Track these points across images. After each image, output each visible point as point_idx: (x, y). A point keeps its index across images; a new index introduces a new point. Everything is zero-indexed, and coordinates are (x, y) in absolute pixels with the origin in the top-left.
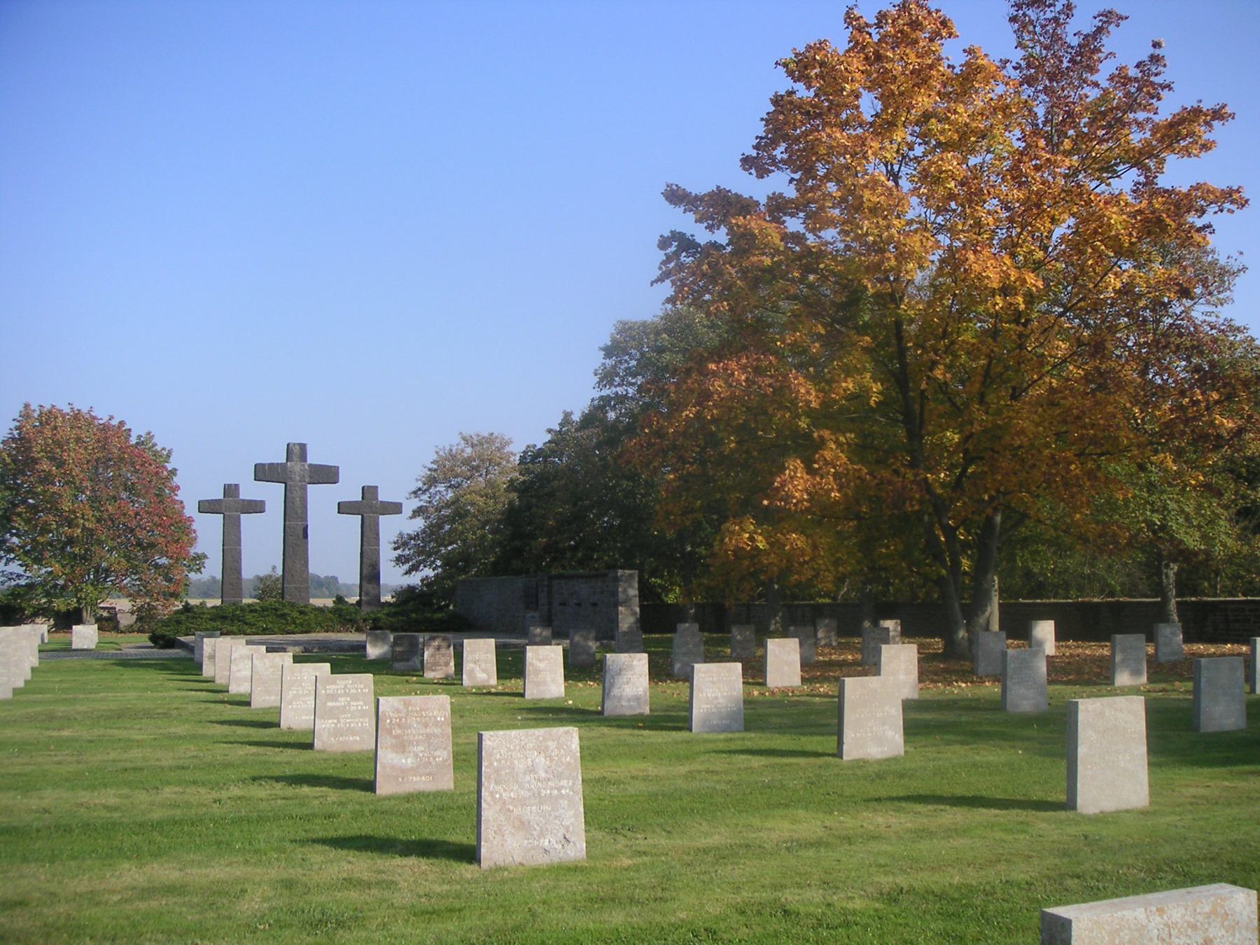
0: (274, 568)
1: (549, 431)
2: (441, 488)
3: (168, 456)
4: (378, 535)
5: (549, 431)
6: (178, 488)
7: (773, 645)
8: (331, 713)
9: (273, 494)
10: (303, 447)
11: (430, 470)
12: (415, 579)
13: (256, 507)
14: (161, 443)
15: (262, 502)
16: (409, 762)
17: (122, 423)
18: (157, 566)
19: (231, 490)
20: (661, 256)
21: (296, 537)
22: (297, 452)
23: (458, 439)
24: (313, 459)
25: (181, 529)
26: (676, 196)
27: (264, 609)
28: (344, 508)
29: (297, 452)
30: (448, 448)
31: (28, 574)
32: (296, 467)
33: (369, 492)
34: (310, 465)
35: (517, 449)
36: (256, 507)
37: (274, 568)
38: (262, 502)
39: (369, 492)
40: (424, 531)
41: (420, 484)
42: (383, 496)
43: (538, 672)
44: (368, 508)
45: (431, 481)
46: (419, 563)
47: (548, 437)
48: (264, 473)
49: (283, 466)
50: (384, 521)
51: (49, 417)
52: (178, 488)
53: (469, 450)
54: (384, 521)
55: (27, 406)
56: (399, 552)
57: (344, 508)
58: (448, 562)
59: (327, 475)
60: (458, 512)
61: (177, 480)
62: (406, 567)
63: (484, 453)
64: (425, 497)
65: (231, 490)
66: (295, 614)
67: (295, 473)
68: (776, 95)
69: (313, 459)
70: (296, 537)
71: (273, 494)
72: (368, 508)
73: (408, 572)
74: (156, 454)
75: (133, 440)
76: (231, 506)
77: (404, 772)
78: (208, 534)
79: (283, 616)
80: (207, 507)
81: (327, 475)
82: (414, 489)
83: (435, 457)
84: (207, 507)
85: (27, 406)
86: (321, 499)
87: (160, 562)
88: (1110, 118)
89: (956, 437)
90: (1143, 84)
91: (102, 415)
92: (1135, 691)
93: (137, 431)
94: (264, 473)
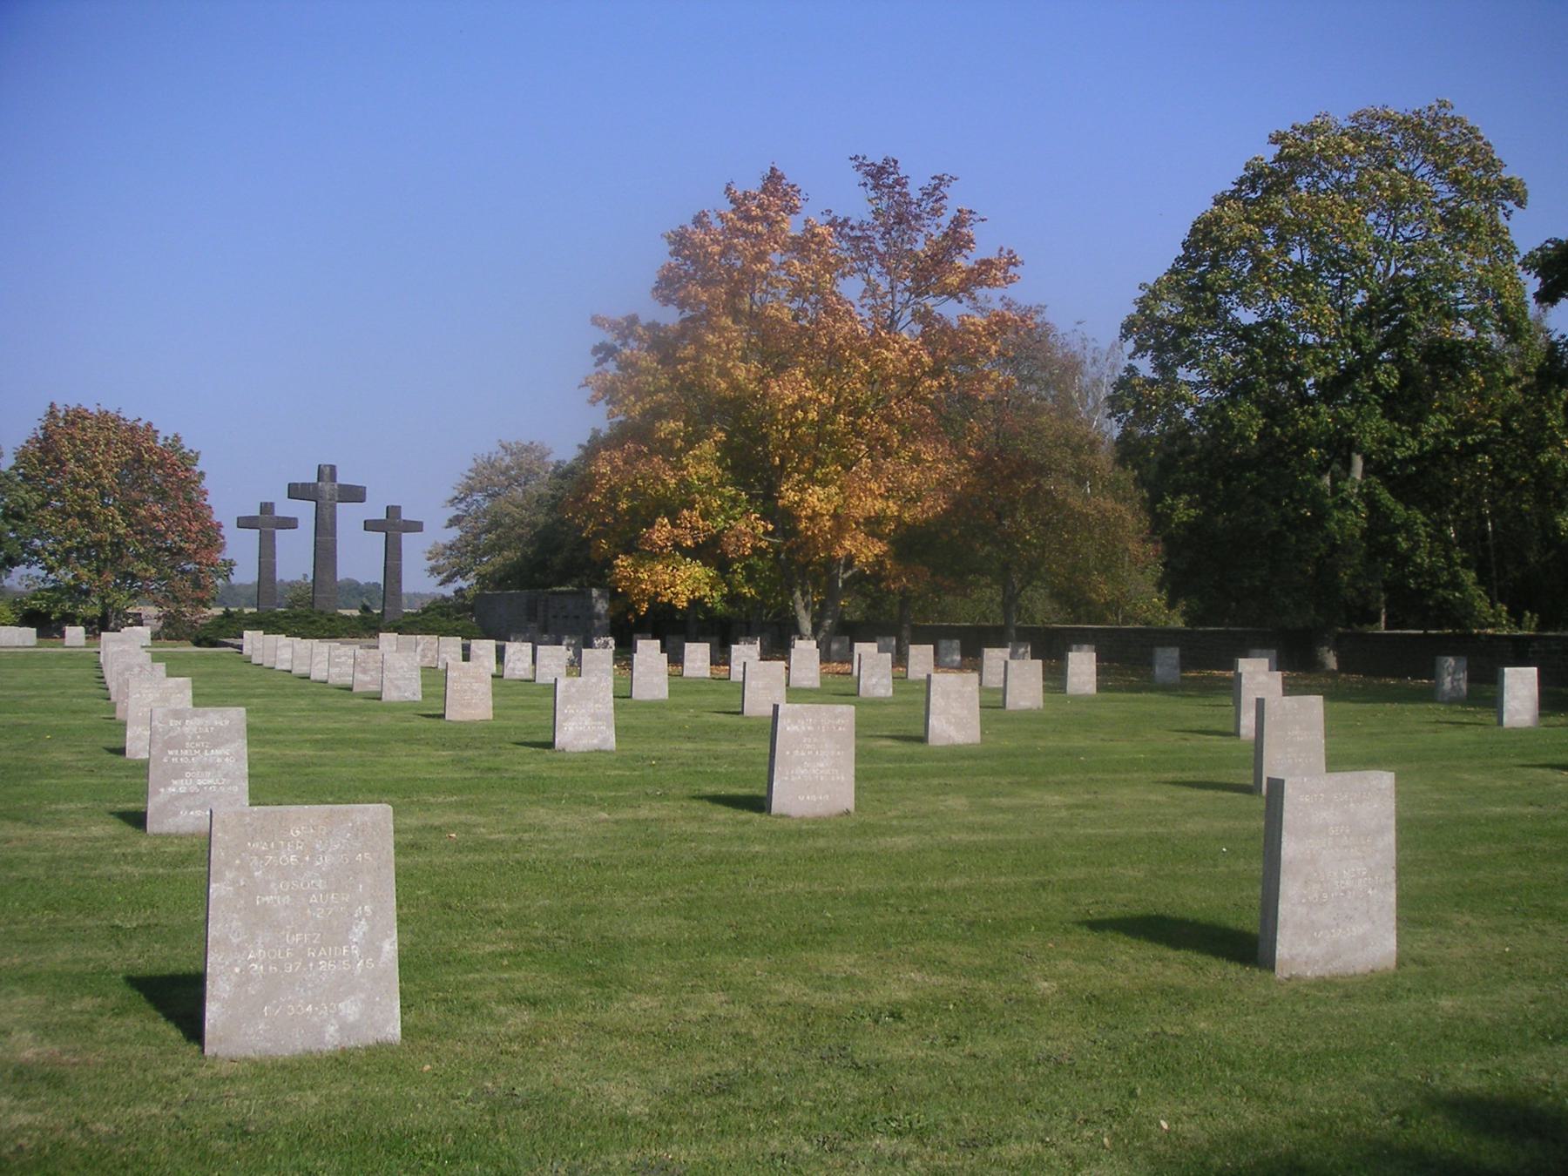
0: (305, 576)
6: (206, 493)
7: (689, 647)
8: (337, 665)
9: (304, 511)
10: (333, 468)
12: (449, 591)
13: (290, 523)
14: (188, 445)
15: (295, 519)
16: (368, 678)
17: (150, 425)
18: (183, 572)
19: (267, 508)
20: (595, 360)
21: (325, 552)
22: (327, 472)
24: (342, 479)
25: (211, 537)
26: (596, 321)
27: (295, 616)
28: (370, 526)
29: (327, 472)
31: (52, 576)
32: (326, 487)
33: (393, 511)
35: (552, 459)
36: (290, 523)
37: (305, 576)
38: (295, 519)
39: (393, 511)
41: (456, 493)
42: (405, 516)
43: (478, 657)
44: (393, 526)
45: (471, 490)
47: (581, 452)
48: (297, 491)
50: (406, 538)
51: (77, 418)
52: (206, 493)
53: (508, 459)
54: (406, 538)
56: (433, 562)
57: (370, 526)
59: (355, 494)
61: (205, 485)
64: (462, 506)
65: (267, 508)
66: (324, 621)
67: (326, 493)
68: (333, 468)
69: (342, 479)
70: (325, 552)
71: (304, 511)
72: (393, 526)
74: (184, 457)
75: (161, 442)
76: (266, 523)
77: (366, 683)
78: (241, 549)
79: (313, 622)
80: (245, 523)
81: (355, 494)
82: (450, 497)
83: (474, 465)
84: (245, 523)
85: (52, 405)
86: (349, 517)
87: (187, 567)
88: (940, 258)
89: (792, 496)
90: (956, 239)
91: (129, 415)
93: (165, 431)
94: (297, 491)
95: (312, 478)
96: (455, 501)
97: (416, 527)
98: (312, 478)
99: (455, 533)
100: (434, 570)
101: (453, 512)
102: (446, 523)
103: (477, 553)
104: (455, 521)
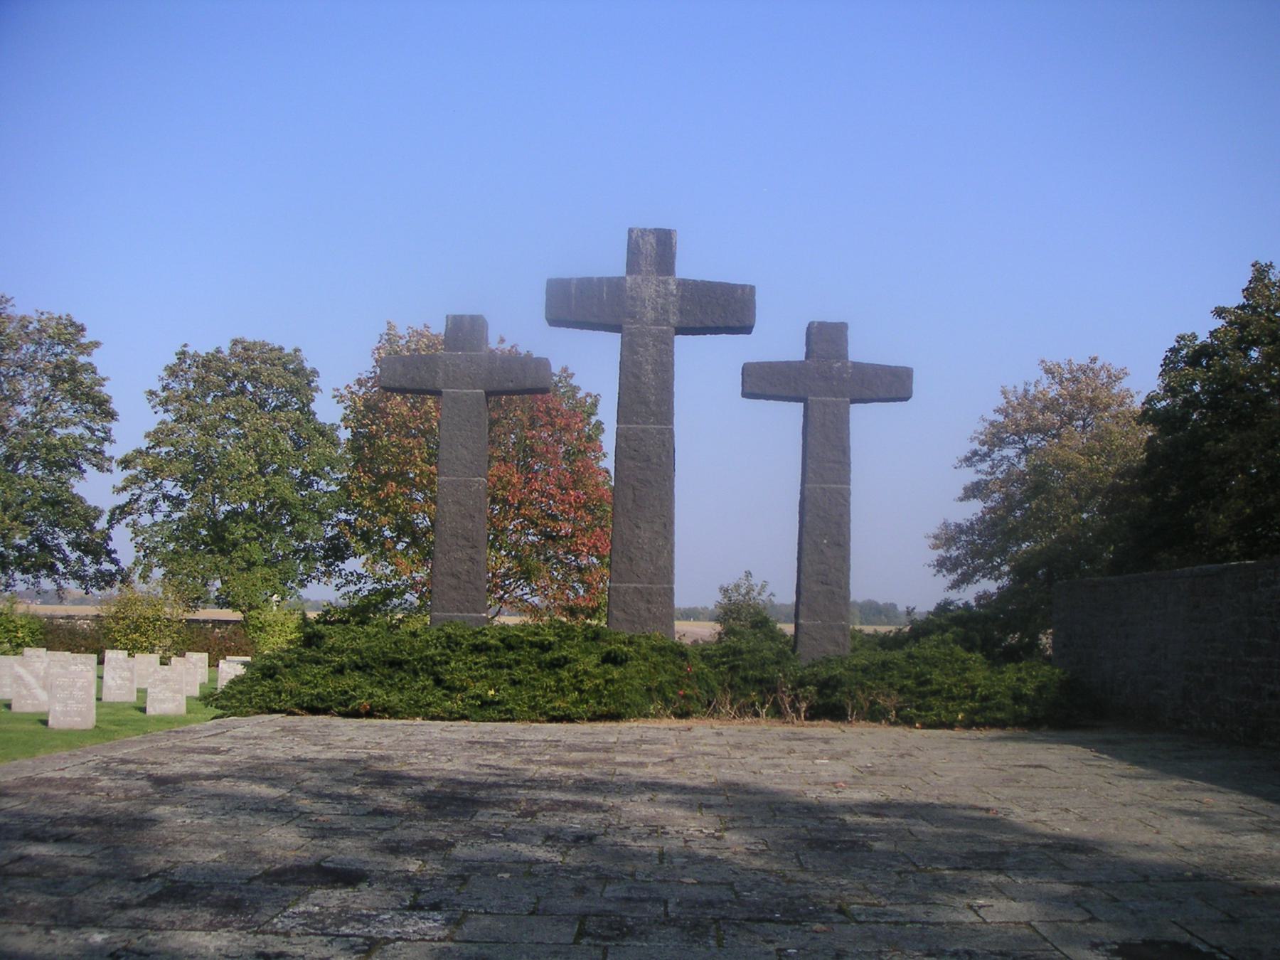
1: (1220, 312)
2: (1010, 452)
3: (595, 405)
4: (845, 451)
5: (1220, 312)
11: (992, 424)
12: (968, 595)
22: (655, 250)
23: (1039, 373)
30: (1020, 391)
33: (826, 338)
34: (683, 284)
35: (1142, 381)
39: (826, 338)
40: (981, 520)
41: (976, 446)
42: (861, 350)
45: (996, 438)
46: (976, 570)
49: (615, 285)
54: (867, 422)
55: (390, 326)
57: (762, 382)
58: (1023, 571)
59: (724, 310)
60: (1037, 483)
62: (954, 576)
63: (1081, 395)
64: (985, 466)
66: (589, 662)
72: (827, 385)
73: (955, 585)
74: (582, 403)
81: (724, 310)
83: (1001, 402)
85: (390, 326)
92: (690, 615)
94: (575, 305)
95: (613, 264)
96: (971, 459)
97: (892, 385)
98: (613, 264)
99: (975, 508)
100: (942, 564)
101: (970, 476)
102: (960, 493)
103: (1013, 535)
104: (973, 491)
